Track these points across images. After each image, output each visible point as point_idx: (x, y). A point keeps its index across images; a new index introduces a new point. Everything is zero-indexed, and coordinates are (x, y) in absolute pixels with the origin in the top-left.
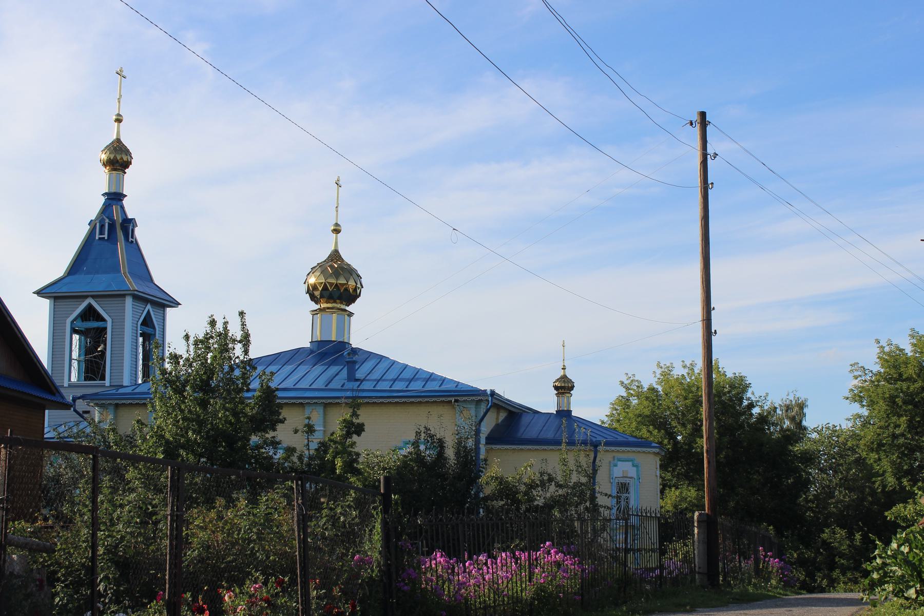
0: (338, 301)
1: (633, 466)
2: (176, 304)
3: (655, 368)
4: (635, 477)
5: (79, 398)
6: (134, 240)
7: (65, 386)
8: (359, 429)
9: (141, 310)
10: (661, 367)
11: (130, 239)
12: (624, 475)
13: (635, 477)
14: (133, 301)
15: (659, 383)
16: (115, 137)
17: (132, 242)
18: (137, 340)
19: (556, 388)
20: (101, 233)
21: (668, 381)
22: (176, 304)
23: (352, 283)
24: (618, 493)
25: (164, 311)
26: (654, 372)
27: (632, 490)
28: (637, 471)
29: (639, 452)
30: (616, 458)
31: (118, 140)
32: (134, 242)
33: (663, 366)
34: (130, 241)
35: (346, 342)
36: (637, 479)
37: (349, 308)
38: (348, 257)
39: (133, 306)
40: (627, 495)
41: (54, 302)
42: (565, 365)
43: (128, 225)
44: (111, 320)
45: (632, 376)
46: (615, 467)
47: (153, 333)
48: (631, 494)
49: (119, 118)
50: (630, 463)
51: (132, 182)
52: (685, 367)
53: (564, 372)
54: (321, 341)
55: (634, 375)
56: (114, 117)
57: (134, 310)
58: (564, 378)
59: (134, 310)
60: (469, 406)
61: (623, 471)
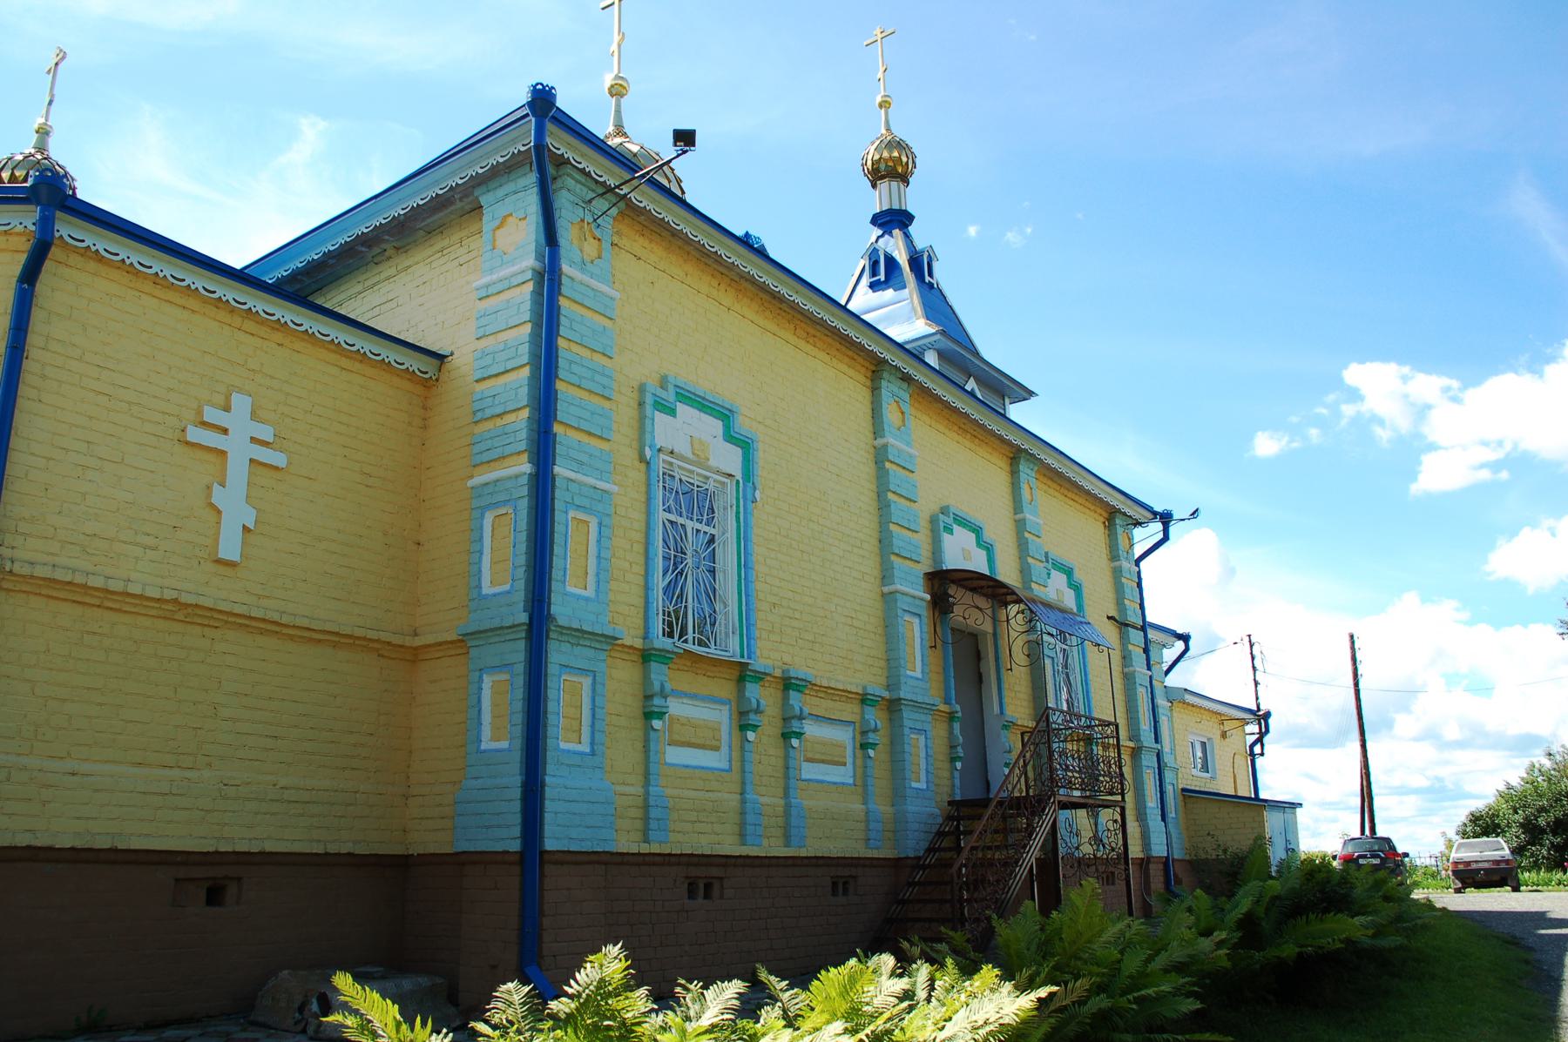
11: (927, 279)
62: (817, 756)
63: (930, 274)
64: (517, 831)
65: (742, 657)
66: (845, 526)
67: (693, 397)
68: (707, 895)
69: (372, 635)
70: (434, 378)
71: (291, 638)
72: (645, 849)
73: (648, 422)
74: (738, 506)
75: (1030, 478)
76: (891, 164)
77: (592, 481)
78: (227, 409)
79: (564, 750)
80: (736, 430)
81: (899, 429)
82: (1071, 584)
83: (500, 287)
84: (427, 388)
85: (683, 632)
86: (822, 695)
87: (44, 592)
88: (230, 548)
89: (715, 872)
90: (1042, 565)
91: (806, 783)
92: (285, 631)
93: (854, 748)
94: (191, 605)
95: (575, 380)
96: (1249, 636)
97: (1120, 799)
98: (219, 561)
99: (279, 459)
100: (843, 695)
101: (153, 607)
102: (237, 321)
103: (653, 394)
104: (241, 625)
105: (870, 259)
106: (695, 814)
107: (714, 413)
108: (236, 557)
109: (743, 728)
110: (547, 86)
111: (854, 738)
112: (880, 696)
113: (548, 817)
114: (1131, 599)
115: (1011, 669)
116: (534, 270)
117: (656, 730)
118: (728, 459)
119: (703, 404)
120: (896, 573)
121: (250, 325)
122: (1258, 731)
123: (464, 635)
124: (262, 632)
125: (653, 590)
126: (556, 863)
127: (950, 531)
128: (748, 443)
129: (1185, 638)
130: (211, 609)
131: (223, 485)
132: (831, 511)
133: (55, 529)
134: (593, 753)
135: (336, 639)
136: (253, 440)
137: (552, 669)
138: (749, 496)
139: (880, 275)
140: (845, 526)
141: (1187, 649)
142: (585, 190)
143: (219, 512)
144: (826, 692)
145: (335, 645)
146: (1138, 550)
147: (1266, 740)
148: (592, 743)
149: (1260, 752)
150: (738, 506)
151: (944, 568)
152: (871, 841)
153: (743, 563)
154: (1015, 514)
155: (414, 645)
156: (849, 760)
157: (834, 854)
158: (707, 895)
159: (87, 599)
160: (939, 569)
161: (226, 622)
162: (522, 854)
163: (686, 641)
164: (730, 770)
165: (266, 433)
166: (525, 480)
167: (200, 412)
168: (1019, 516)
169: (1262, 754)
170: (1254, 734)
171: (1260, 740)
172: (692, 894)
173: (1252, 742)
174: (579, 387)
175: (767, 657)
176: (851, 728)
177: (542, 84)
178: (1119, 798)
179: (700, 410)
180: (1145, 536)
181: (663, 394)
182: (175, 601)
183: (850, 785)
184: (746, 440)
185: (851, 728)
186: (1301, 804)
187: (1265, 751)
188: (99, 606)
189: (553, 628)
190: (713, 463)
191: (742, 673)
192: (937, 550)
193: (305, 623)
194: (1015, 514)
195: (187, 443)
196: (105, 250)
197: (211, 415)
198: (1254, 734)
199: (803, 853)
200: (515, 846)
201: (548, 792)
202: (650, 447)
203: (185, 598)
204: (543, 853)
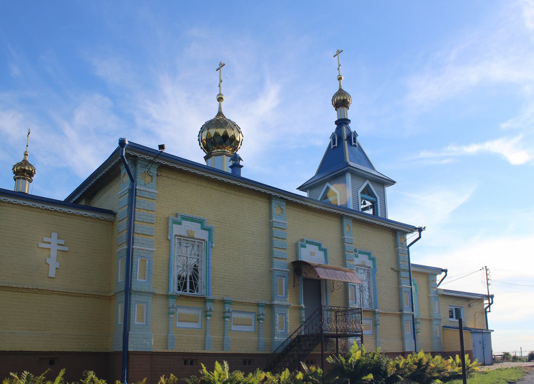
2: (393, 182)
4: (207, 240)
6: (357, 144)
7: (133, 246)
9: (362, 184)
11: (353, 144)
13: (207, 240)
14: (351, 177)
17: (355, 146)
18: (358, 207)
20: (334, 144)
25: (384, 189)
31: (340, 89)
32: (357, 146)
34: (353, 144)
39: (352, 182)
43: (352, 138)
47: (375, 200)
51: (351, 114)
62: (239, 323)
63: (355, 142)
64: (122, 346)
65: (206, 295)
66: (255, 250)
67: (188, 218)
68: (250, 364)
69: (95, 293)
70: (114, 220)
71: (72, 296)
72: (166, 351)
73: (170, 229)
74: (207, 249)
75: (349, 223)
76: (221, 147)
77: (147, 248)
78: (51, 237)
79: (136, 324)
80: (205, 226)
81: (280, 215)
82: (370, 258)
83: (122, 194)
84: (113, 223)
85: (185, 287)
86: (241, 305)
87: (2, 289)
88: (52, 274)
89: (193, 357)
90: (353, 254)
91: (233, 331)
92: (69, 294)
93: (255, 320)
94: (41, 290)
95: (141, 220)
96: (486, 267)
97: (336, 333)
98: (49, 278)
99: (66, 248)
100: (250, 304)
101: (32, 291)
102: (53, 213)
103: (172, 219)
104: (57, 293)
105: (333, 139)
106: (187, 341)
107: (197, 222)
108: (54, 276)
109: (206, 316)
110: (123, 138)
111: (255, 317)
112: (265, 304)
113: (129, 342)
114: (403, 260)
115: (333, 291)
116: (129, 189)
117: (171, 318)
118: (203, 235)
119: (192, 220)
120: (275, 264)
121: (56, 213)
122: (488, 303)
123: (115, 293)
124: (63, 295)
125: (171, 278)
126: (133, 354)
127: (304, 246)
128: (210, 229)
129: (446, 271)
130: (47, 290)
131: (49, 257)
132: (248, 246)
133: (4, 273)
134: (147, 325)
135: (85, 295)
136: (58, 244)
137: (133, 302)
138: (210, 245)
139: (335, 144)
140: (255, 250)
141: (446, 275)
142: (145, 162)
143: (49, 265)
144: (242, 304)
145: (85, 297)
146: (408, 242)
147: (491, 306)
148: (146, 322)
149: (489, 311)
150: (207, 249)
151: (300, 260)
152: (260, 349)
153: (207, 266)
154: (342, 237)
155: (110, 295)
156: (253, 324)
157: (249, 352)
158: (250, 364)
159: (13, 290)
160: (298, 260)
161: (52, 293)
162: (123, 352)
163: (186, 291)
164: (201, 328)
165: (62, 242)
166: (125, 250)
167: (43, 239)
168: (343, 237)
169: (490, 311)
170: (487, 304)
171: (489, 306)
172: (186, 363)
173: (486, 307)
174: (143, 222)
175: (215, 294)
176: (254, 314)
177: (121, 138)
178: (361, 333)
179: (192, 221)
180: (410, 238)
181: (176, 219)
182: (37, 289)
183: (253, 332)
184: (210, 228)
185: (254, 314)
186: (493, 331)
187: (490, 310)
188: (17, 291)
189: (132, 291)
190: (196, 236)
191: (204, 300)
192: (297, 254)
193: (75, 292)
194: (342, 237)
195: (40, 248)
196: (13, 201)
197: (46, 239)
198: (487, 304)
199: (229, 352)
200: (121, 350)
201: (130, 336)
202: (170, 236)
203: (39, 288)
204: (128, 352)
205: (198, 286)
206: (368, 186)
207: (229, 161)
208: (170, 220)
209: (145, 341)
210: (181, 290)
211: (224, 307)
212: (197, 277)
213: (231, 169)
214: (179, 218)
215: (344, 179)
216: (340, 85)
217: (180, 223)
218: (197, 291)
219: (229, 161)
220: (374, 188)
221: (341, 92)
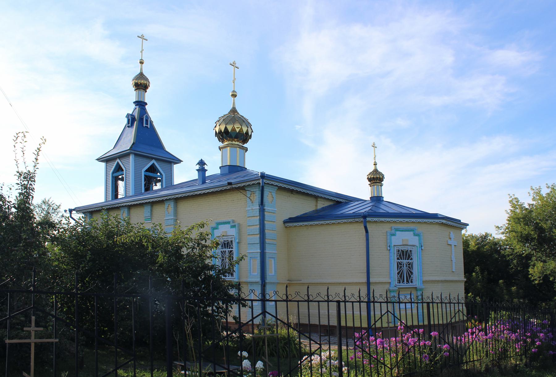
0: (236, 140)
1: (415, 235)
2: (178, 161)
3: (529, 190)
5: (74, 210)
8: (394, 235)
10: (533, 190)
11: (144, 125)
12: (404, 244)
14: (135, 157)
15: (534, 199)
16: (139, 72)
19: (370, 180)
21: (541, 196)
22: (178, 161)
23: (245, 129)
24: (398, 259)
26: (529, 193)
27: (415, 257)
28: (420, 240)
29: (419, 223)
30: (393, 228)
33: (534, 189)
34: (144, 126)
35: (380, 196)
36: (420, 247)
37: (245, 145)
38: (241, 112)
40: (410, 261)
41: (106, 164)
42: (376, 161)
44: (142, 170)
45: (513, 196)
46: (393, 237)
48: (414, 260)
49: (142, 61)
50: (412, 233)
51: (149, 97)
52: (548, 187)
53: (375, 167)
54: (373, 197)
55: (514, 195)
56: (231, 94)
57: (136, 162)
58: (376, 171)
59: (136, 162)
60: (255, 190)
61: (402, 239)
163: (404, 283)
205: (412, 278)
206: (118, 163)
207: (197, 165)
208: (388, 233)
209: (53, 356)
210: (401, 283)
211: (417, 293)
212: (412, 273)
213: (197, 172)
214: (393, 231)
215: (148, 162)
216: (141, 69)
217: (394, 234)
218: (412, 282)
219: (197, 165)
220: (162, 170)
221: (141, 75)
